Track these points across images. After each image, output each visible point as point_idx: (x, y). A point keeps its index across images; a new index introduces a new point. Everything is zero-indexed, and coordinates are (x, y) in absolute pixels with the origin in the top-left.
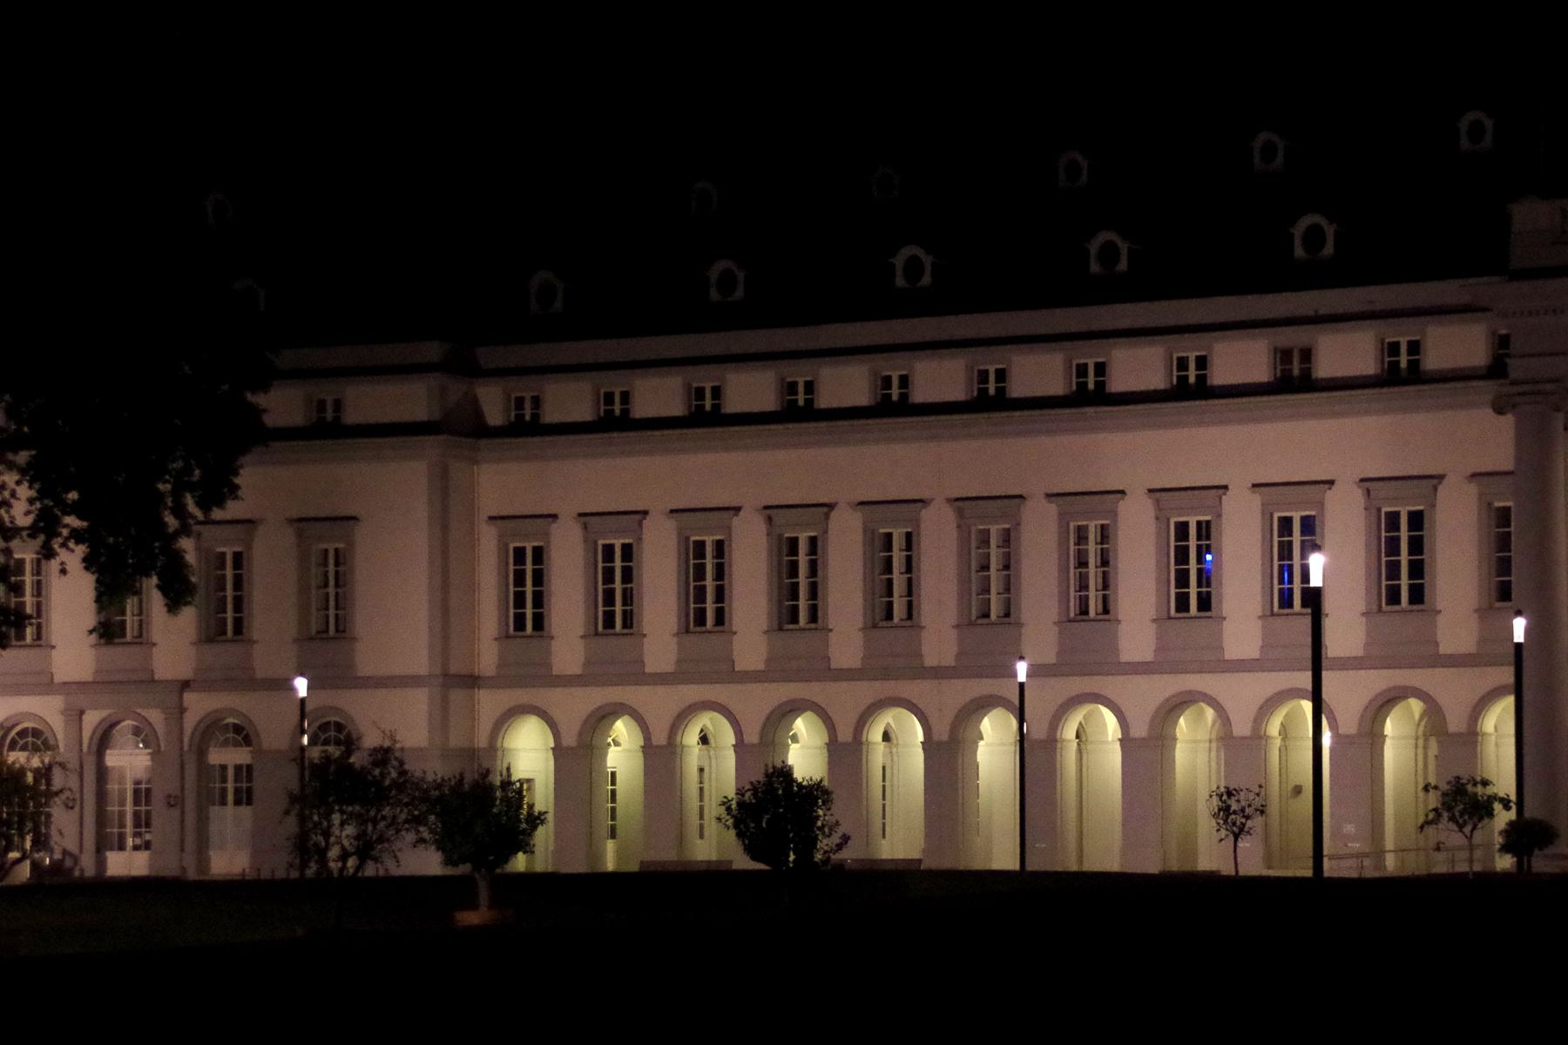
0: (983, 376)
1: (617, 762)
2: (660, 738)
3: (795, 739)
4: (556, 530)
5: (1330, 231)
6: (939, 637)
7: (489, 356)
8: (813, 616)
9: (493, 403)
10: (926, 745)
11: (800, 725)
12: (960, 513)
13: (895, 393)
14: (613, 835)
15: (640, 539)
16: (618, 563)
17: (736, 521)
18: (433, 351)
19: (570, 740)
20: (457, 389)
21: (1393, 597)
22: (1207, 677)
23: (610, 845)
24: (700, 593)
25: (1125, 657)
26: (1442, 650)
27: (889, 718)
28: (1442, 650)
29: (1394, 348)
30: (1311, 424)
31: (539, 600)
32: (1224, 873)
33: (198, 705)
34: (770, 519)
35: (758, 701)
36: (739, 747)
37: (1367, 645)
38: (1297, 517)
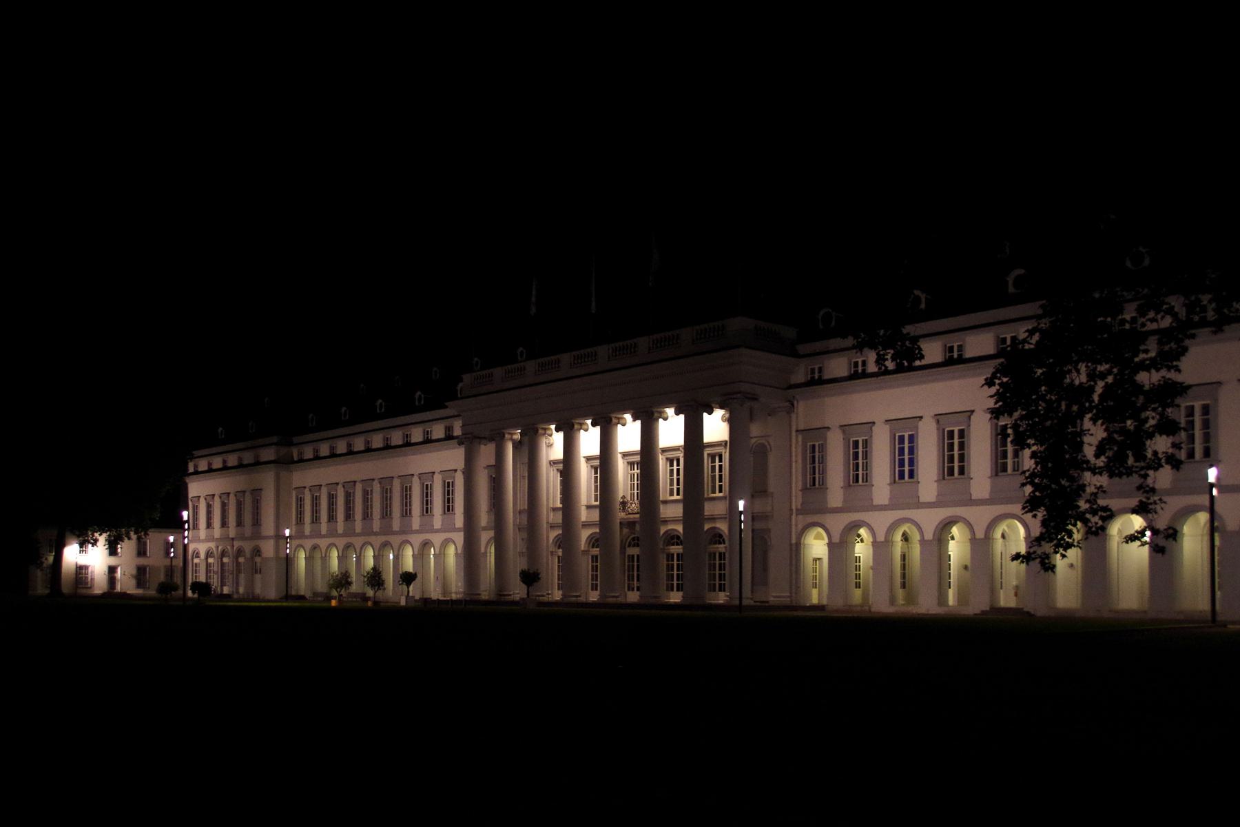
0: (813, 371)
1: (431, 556)
2: (980, 535)
3: (953, 538)
4: (830, 435)
5: (923, 297)
6: (835, 493)
7: (296, 440)
8: (962, 471)
9: (308, 453)
10: (1026, 538)
11: (955, 530)
12: (844, 432)
13: (956, 355)
14: (858, 585)
15: (1216, 400)
16: (906, 445)
17: (921, 423)
18: (275, 439)
19: (836, 539)
20: (284, 451)
21: (951, 473)
22: (915, 511)
23: (815, 592)
24: (951, 459)
25: (876, 502)
26: (922, 500)
27: (1002, 527)
28: (922, 500)
29: (1004, 340)
30: (916, 387)
31: (911, 462)
32: (1039, 614)
33: (237, 544)
34: (938, 422)
35: (930, 519)
36: (923, 542)
37: (992, 492)
38: (956, 430)
